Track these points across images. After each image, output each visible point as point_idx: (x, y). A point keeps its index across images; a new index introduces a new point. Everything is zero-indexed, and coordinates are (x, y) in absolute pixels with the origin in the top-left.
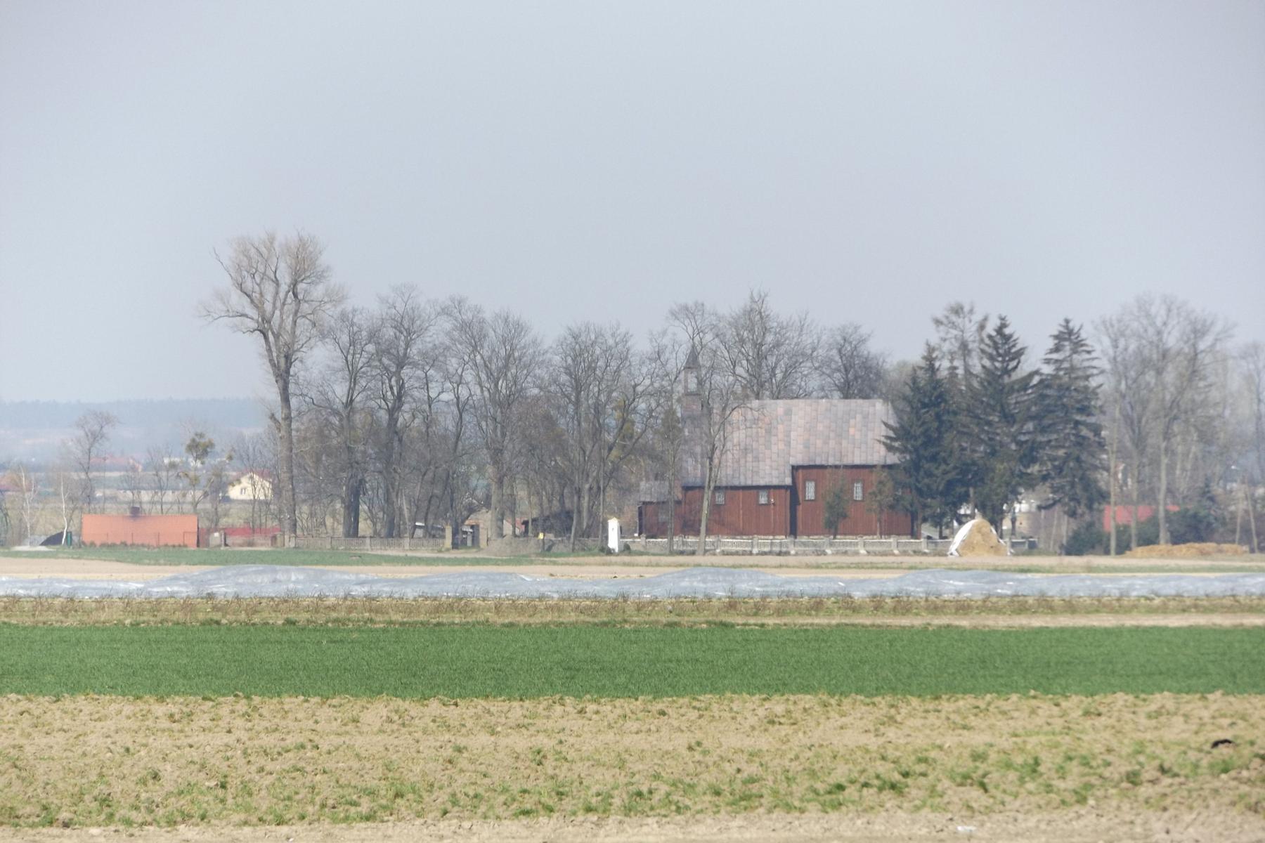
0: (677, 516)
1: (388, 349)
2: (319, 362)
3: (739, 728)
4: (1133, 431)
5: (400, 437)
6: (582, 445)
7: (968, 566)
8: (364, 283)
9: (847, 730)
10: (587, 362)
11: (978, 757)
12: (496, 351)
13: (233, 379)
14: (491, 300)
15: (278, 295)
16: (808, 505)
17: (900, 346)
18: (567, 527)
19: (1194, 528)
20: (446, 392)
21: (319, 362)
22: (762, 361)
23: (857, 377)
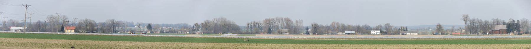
0: (492, 32)
1: (473, 22)
2: (468, 22)
4: (193, 30)
6: (486, 28)
7: (512, 36)
8: (471, 17)
12: (480, 22)
14: (479, 19)
15: (466, 18)
16: (501, 32)
17: (507, 21)
18: (485, 33)
19: (526, 33)
21: (468, 22)
22: (498, 22)
23: (504, 23)
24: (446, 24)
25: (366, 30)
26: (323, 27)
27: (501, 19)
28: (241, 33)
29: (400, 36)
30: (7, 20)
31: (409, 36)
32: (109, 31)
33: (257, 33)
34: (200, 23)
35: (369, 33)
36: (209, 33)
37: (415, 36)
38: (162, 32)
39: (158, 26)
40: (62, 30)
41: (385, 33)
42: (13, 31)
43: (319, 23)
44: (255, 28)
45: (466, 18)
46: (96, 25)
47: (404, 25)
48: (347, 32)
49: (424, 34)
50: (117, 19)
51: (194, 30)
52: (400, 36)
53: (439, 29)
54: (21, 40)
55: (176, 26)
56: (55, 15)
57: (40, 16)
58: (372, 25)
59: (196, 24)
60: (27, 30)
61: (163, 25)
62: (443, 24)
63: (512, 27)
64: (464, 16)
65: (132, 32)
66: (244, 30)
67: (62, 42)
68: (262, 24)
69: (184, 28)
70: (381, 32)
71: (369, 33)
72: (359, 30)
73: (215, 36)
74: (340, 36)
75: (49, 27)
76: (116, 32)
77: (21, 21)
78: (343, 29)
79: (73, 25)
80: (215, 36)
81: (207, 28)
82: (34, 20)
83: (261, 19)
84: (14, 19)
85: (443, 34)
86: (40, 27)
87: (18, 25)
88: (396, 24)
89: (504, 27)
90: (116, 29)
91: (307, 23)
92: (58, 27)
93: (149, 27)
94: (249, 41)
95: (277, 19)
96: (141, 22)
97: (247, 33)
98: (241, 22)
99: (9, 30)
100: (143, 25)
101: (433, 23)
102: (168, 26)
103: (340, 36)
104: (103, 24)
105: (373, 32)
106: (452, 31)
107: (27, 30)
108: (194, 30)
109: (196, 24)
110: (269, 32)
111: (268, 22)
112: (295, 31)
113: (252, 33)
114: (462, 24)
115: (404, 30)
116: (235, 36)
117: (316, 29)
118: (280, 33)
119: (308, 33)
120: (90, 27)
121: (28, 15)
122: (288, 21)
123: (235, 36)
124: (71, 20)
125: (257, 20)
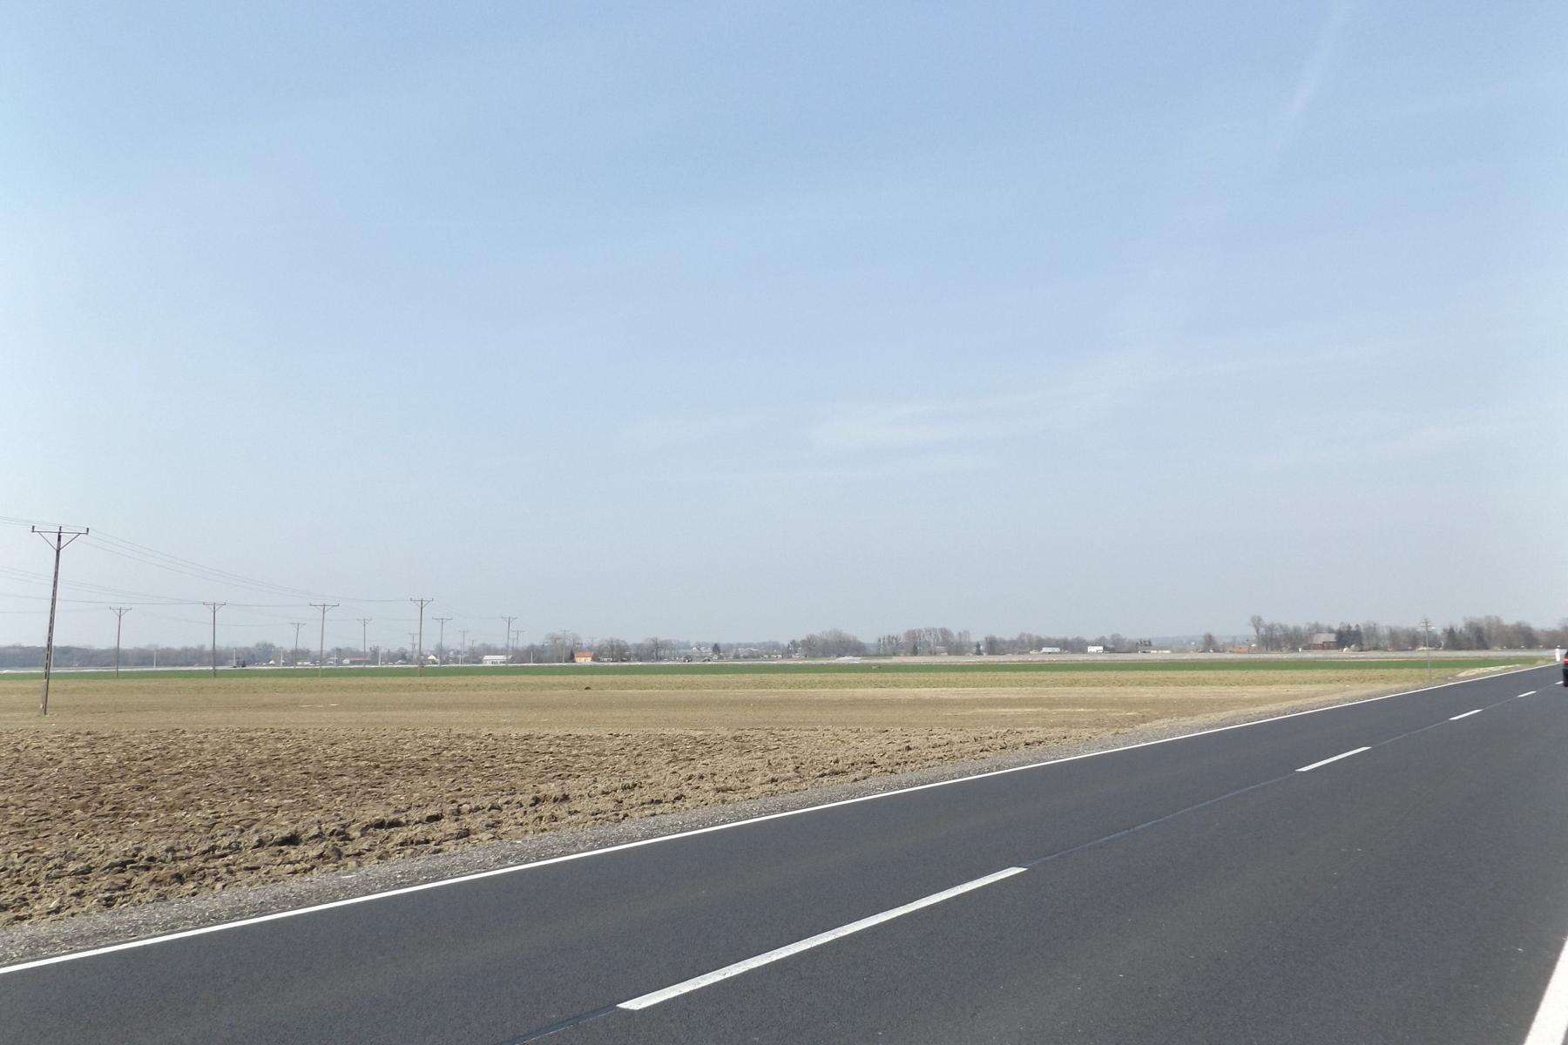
0: (1307, 648)
1: (1271, 628)
2: (1262, 630)
3: (1318, 674)
4: (787, 653)
5: (1270, 640)
6: (1295, 640)
7: (1346, 653)
8: (1267, 621)
9: (1332, 674)
10: (1296, 630)
11: (162, 897)
12: (1284, 629)
13: (1252, 632)
14: (1283, 623)
15: (1257, 622)
16: (1325, 646)
17: (1336, 627)
18: (1295, 649)
19: (1376, 648)
20: (1278, 633)
21: (1262, 630)
22: (1318, 629)
23: (1330, 631)
24: (1221, 632)
25: (1079, 646)
26: (1004, 642)
27: (1325, 622)
28: (866, 655)
29: (1139, 656)
30: (476, 644)
31: (1154, 655)
32: (649, 658)
33: (895, 654)
34: (798, 640)
35: (1084, 651)
36: (814, 657)
37: (1166, 654)
38: (737, 657)
39: (730, 647)
40: (572, 658)
41: (1112, 651)
42: (488, 664)
43: (998, 635)
44: (892, 647)
45: (1257, 622)
46: (627, 648)
47: (1146, 636)
48: (1045, 650)
49: (1181, 651)
50: (662, 638)
51: (789, 652)
52: (1139, 656)
53: (1209, 643)
54: (501, 680)
55: (758, 646)
56: (559, 633)
57: (534, 635)
58: (1089, 637)
59: (793, 643)
60: (511, 661)
61: (739, 645)
62: (1215, 633)
63: (1346, 638)
64: (1253, 619)
65: (689, 658)
66: (873, 650)
67: (571, 679)
68: (903, 640)
69: (772, 649)
70: (1105, 649)
71: (1084, 651)
72: (1066, 645)
73: (824, 661)
74: (1034, 657)
75: (548, 654)
76: (661, 659)
77: (500, 645)
78: (1039, 644)
79: (590, 649)
80: (824, 661)
81: (811, 647)
82: (523, 643)
83: (899, 630)
84: (488, 642)
85: (1216, 651)
86: (535, 654)
87: (496, 652)
88: (1131, 634)
89: (1332, 638)
90: (662, 653)
91: (978, 636)
92: (565, 654)
93: (716, 648)
94: (881, 669)
95: (929, 631)
96: (701, 640)
97: (877, 655)
98: (868, 637)
99: (480, 661)
100: (706, 646)
101: (1197, 631)
102: (746, 646)
103: (1034, 657)
104: (639, 647)
105: (1091, 649)
106: (1233, 646)
107: (511, 661)
108: (789, 652)
109: (793, 643)
110: (915, 652)
111: (912, 635)
112: (957, 649)
113: (886, 655)
114: (1251, 632)
115: (1146, 645)
116: (857, 660)
117: (993, 646)
118: (933, 653)
119: (979, 653)
120: (619, 652)
121: (512, 635)
122: (945, 632)
123: (857, 660)
124: (585, 641)
125: (894, 633)
